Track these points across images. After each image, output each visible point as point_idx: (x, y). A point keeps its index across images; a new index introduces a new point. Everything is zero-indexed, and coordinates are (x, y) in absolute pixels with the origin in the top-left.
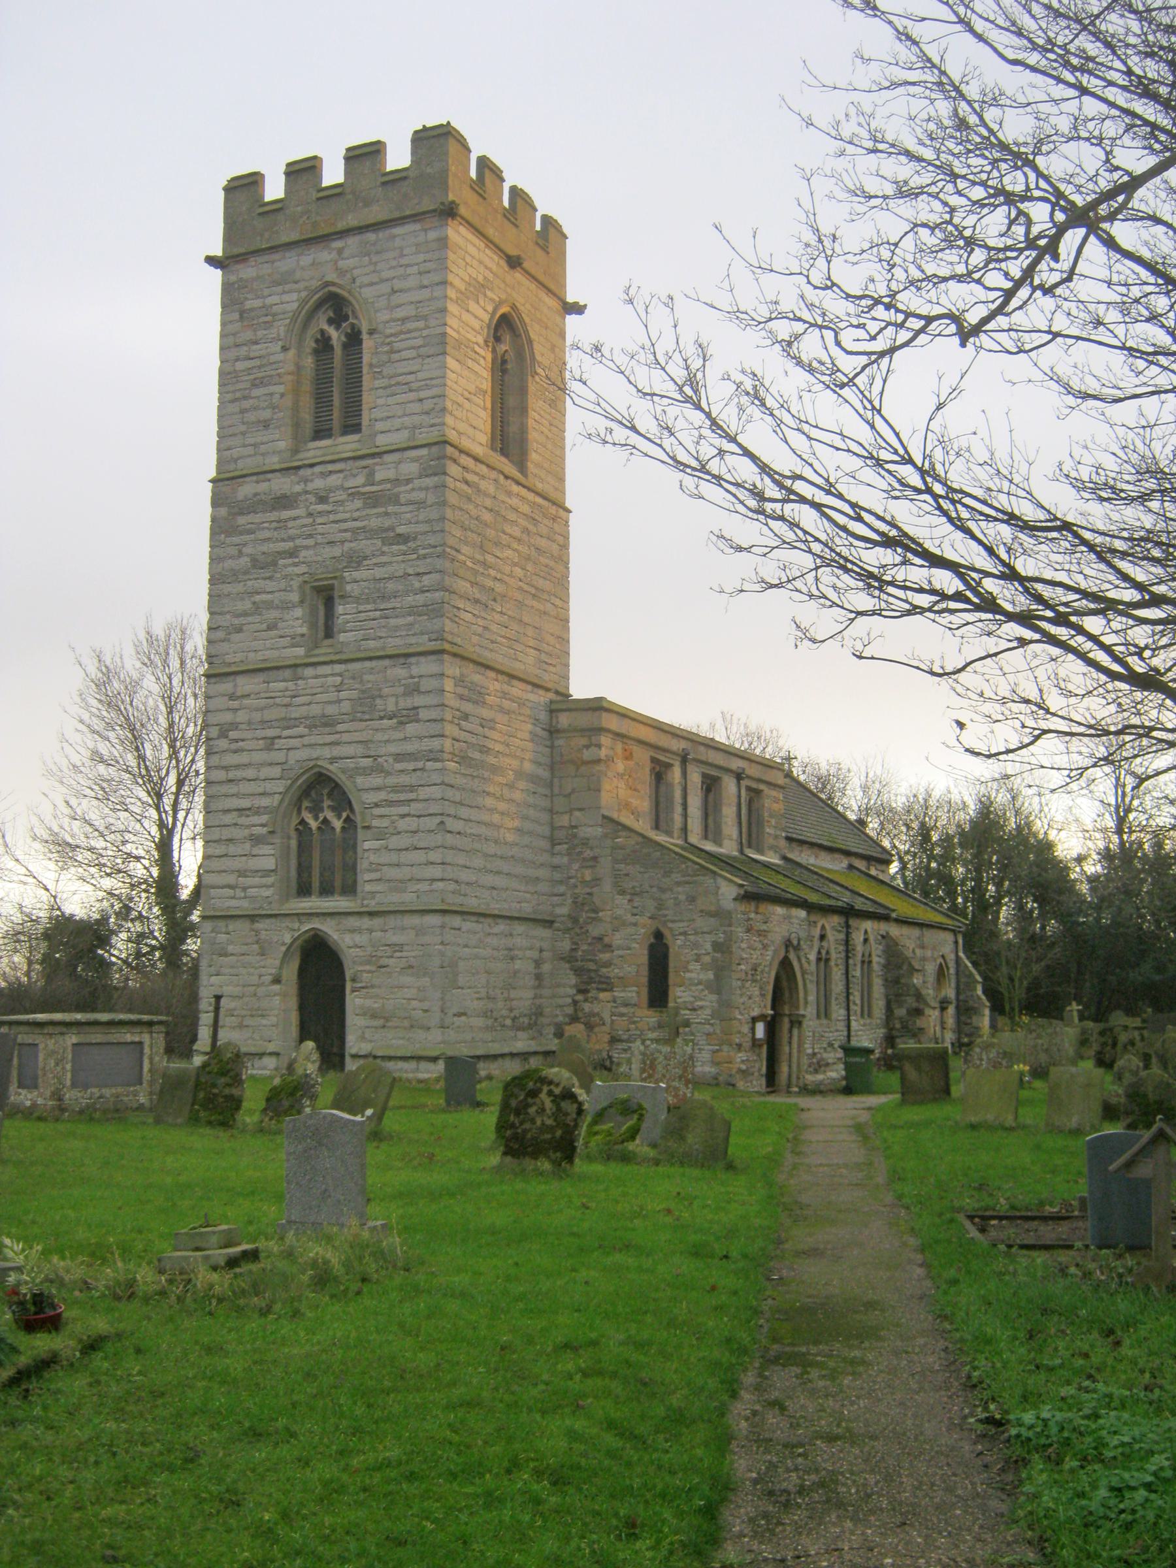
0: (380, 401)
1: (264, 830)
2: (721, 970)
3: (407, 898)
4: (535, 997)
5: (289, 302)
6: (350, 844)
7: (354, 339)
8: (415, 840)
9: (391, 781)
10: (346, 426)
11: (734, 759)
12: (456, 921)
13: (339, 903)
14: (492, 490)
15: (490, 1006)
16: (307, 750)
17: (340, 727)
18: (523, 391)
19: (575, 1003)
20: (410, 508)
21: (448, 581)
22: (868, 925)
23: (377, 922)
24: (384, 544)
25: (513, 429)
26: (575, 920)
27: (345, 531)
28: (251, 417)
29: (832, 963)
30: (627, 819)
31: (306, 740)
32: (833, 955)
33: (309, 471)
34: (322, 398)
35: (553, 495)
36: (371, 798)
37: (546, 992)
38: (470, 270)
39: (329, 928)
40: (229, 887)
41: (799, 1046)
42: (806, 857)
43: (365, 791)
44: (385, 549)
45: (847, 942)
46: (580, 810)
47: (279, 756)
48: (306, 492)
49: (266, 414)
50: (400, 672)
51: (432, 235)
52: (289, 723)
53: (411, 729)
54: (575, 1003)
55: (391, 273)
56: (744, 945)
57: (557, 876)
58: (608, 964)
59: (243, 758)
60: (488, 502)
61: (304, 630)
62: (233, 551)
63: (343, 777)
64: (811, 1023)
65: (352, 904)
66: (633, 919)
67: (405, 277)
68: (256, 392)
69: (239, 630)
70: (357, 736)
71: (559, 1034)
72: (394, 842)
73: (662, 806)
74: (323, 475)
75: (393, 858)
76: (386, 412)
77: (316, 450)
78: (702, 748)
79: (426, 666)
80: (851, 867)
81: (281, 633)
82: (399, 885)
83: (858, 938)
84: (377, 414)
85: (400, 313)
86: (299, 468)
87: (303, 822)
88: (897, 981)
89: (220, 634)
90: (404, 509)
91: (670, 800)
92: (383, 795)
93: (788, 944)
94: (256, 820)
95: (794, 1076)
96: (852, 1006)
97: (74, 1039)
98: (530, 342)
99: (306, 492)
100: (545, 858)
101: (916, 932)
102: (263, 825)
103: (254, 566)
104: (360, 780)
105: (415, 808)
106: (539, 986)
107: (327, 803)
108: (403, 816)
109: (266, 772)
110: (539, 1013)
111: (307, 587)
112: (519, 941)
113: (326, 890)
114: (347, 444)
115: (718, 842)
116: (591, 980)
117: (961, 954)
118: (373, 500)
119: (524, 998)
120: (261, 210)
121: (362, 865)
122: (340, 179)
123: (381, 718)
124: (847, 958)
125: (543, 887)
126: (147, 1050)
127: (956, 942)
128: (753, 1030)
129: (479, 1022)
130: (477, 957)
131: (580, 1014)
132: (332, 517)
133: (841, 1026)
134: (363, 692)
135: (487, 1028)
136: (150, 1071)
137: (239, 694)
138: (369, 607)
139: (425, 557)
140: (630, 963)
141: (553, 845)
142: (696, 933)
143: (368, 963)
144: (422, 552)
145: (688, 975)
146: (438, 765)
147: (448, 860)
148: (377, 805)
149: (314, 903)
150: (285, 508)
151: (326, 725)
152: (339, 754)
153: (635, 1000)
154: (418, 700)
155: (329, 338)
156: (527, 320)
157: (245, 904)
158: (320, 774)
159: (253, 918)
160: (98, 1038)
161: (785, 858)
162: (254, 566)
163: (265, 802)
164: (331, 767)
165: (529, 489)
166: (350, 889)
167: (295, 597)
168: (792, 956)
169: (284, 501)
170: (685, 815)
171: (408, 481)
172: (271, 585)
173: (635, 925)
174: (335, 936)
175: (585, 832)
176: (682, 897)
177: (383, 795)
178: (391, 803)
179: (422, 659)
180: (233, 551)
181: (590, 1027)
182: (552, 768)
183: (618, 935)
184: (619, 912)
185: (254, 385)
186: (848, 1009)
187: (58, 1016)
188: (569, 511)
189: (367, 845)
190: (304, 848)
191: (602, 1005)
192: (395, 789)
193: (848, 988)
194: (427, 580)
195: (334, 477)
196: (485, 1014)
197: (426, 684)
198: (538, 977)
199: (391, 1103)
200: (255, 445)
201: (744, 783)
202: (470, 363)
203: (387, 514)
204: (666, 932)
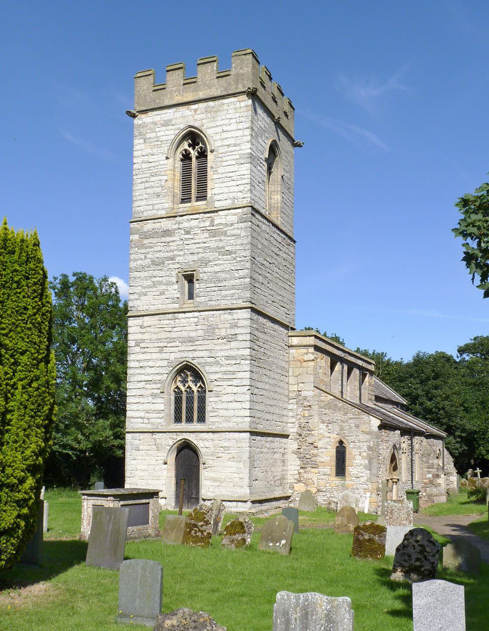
7: (202, 155)
13: (196, 426)
16: (178, 355)
39: (191, 438)
43: (210, 373)
72: (224, 398)
82: (227, 419)
93: (394, 447)
113: (190, 420)
116: (307, 462)
166: (202, 419)
169: (167, 233)
190: (178, 401)
191: (312, 475)
192: (225, 373)
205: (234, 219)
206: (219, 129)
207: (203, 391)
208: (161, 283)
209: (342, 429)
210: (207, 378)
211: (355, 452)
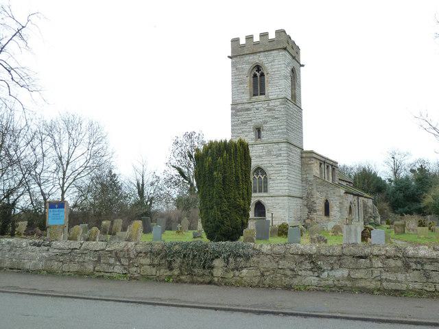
2: (341, 208)
3: (280, 193)
5: (247, 67)
6: (266, 182)
7: (262, 75)
13: (265, 194)
23: (273, 198)
34: (255, 87)
39: (262, 200)
43: (269, 171)
72: (276, 182)
82: (278, 190)
88: (365, 210)
113: (260, 191)
114: (262, 97)
116: (311, 210)
118: (270, 110)
122: (244, 43)
140: (320, 206)
166: (266, 191)
169: (248, 110)
175: (309, 179)
191: (314, 215)
208: (245, 131)
211: (334, 205)
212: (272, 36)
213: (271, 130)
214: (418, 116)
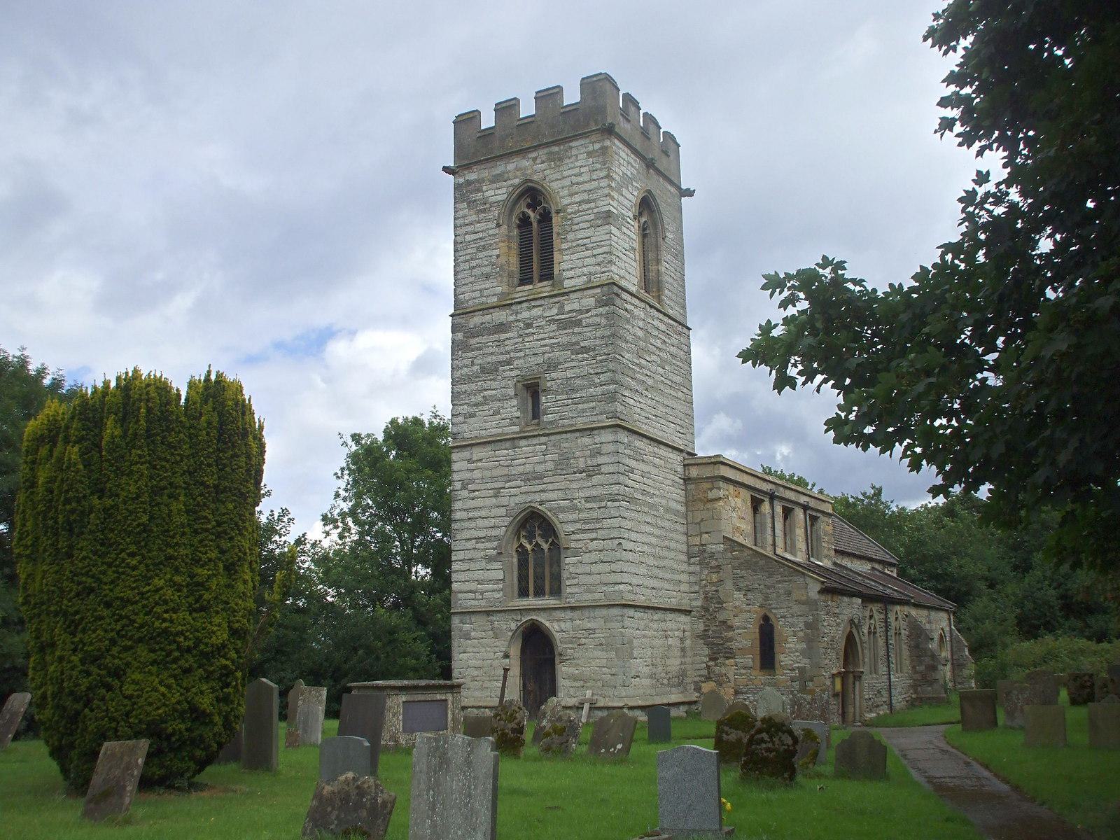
0: (565, 258)
1: (494, 552)
3: (598, 596)
4: (682, 663)
5: (497, 194)
6: (556, 562)
7: (546, 218)
8: (601, 556)
9: (585, 515)
10: (541, 276)
11: (801, 496)
12: (631, 612)
13: (549, 601)
14: (642, 316)
15: (654, 670)
16: (519, 497)
17: (546, 480)
18: (657, 248)
19: (708, 667)
20: (591, 328)
21: (619, 377)
22: (898, 608)
23: (576, 614)
24: (572, 354)
25: (652, 275)
26: (707, 610)
27: (545, 346)
28: (477, 272)
29: (878, 635)
30: (740, 540)
31: (523, 489)
32: (878, 630)
33: (519, 307)
35: (679, 318)
36: (570, 528)
37: (687, 660)
38: (622, 168)
39: (542, 619)
40: (471, 591)
41: (860, 693)
42: (847, 562)
43: (565, 525)
44: (573, 357)
45: (886, 622)
46: (707, 533)
47: (505, 501)
48: (517, 321)
49: (488, 269)
50: (587, 440)
51: (597, 146)
52: (509, 478)
53: (596, 479)
54: (708, 667)
55: (570, 172)
56: (825, 624)
57: (693, 579)
58: (730, 640)
59: (479, 503)
60: (641, 324)
61: (518, 414)
62: (469, 362)
63: (549, 514)
64: (867, 679)
65: (558, 602)
66: (747, 608)
67: (580, 174)
68: (481, 255)
69: (472, 415)
70: (556, 486)
71: (698, 689)
72: (586, 558)
73: (758, 528)
74: (530, 309)
75: (587, 569)
76: (572, 264)
77: (524, 291)
78: (781, 489)
79: (607, 436)
80: (873, 569)
81: (503, 416)
82: (590, 587)
83: (892, 617)
84: (564, 266)
85: (577, 198)
86: (512, 304)
87: (521, 546)
88: (917, 647)
89: (461, 419)
90: (585, 329)
91: (763, 525)
92: (578, 526)
93: (851, 621)
94: (488, 545)
95: (857, 714)
96: (892, 665)
97: (404, 699)
98: (660, 214)
99: (517, 321)
100: (684, 567)
101: (925, 612)
102: (494, 549)
103: (483, 372)
104: (561, 516)
105: (601, 534)
106: (684, 656)
107: (538, 532)
108: (592, 540)
109: (495, 512)
110: (683, 674)
111: (519, 385)
112: (670, 625)
113: (539, 592)
114: (544, 288)
115: (794, 555)
116: (719, 649)
117: (953, 627)
118: (564, 325)
119: (674, 663)
120: (518, 123)
121: (565, 575)
123: (575, 473)
124: (887, 631)
125: (684, 587)
126: (450, 705)
127: (949, 619)
128: (833, 683)
129: (646, 682)
130: (645, 636)
131: (712, 675)
132: (536, 337)
133: (885, 679)
134: (562, 455)
135: (653, 686)
136: (453, 719)
137: (474, 459)
138: (563, 397)
139: (601, 361)
140: (745, 637)
141: (689, 558)
142: (793, 616)
143: (571, 642)
144: (599, 358)
145: (788, 646)
146: (616, 504)
147: (625, 570)
148: (573, 533)
149: (532, 602)
150: (502, 332)
151: (535, 479)
152: (549, 498)
153: (751, 664)
154: (600, 460)
155: (529, 217)
156: (658, 201)
157: (483, 603)
158: (533, 512)
159: (488, 613)
160: (420, 697)
161: (835, 564)
162: (483, 372)
163: (495, 532)
164: (540, 507)
165: (665, 314)
166: (557, 591)
167: (511, 392)
168: (854, 631)
169: (501, 327)
170: (774, 536)
171: (588, 311)
172: (495, 384)
173: (749, 612)
174: (547, 624)
175: (712, 548)
176: (782, 591)
177: (578, 526)
178: (583, 531)
179: (602, 431)
180: (469, 362)
181: (720, 684)
182: (686, 504)
183: (737, 619)
184: (737, 603)
185: (479, 250)
186: (889, 667)
187: (392, 682)
188: (690, 329)
189: (567, 561)
190: (523, 564)
191: (728, 669)
192: (586, 521)
193: (888, 652)
194: (603, 378)
195: (536, 309)
196: (651, 677)
197: (606, 449)
198: (683, 650)
199: (635, 737)
200: (481, 290)
201: (808, 512)
202: (625, 230)
203: (573, 333)
204: (771, 616)
205: (592, 301)
206: (567, 182)
207: (556, 547)
209: (766, 598)
210: (563, 529)
211: (789, 631)
212: (572, 96)
213: (568, 388)
214: (939, 134)
